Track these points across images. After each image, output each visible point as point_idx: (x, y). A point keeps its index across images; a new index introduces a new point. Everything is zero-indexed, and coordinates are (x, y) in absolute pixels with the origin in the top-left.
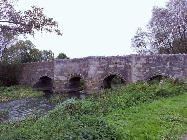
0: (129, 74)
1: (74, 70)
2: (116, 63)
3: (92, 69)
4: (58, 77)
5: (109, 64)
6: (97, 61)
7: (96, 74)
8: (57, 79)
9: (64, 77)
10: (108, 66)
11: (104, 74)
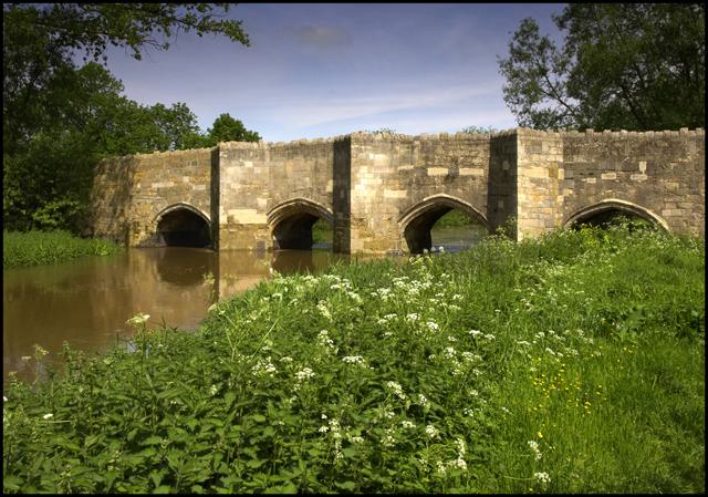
1: (295, 186)
3: (363, 181)
4: (231, 212)
5: (428, 166)
6: (384, 151)
7: (379, 201)
8: (230, 219)
9: (254, 212)
10: (424, 169)
11: (409, 202)
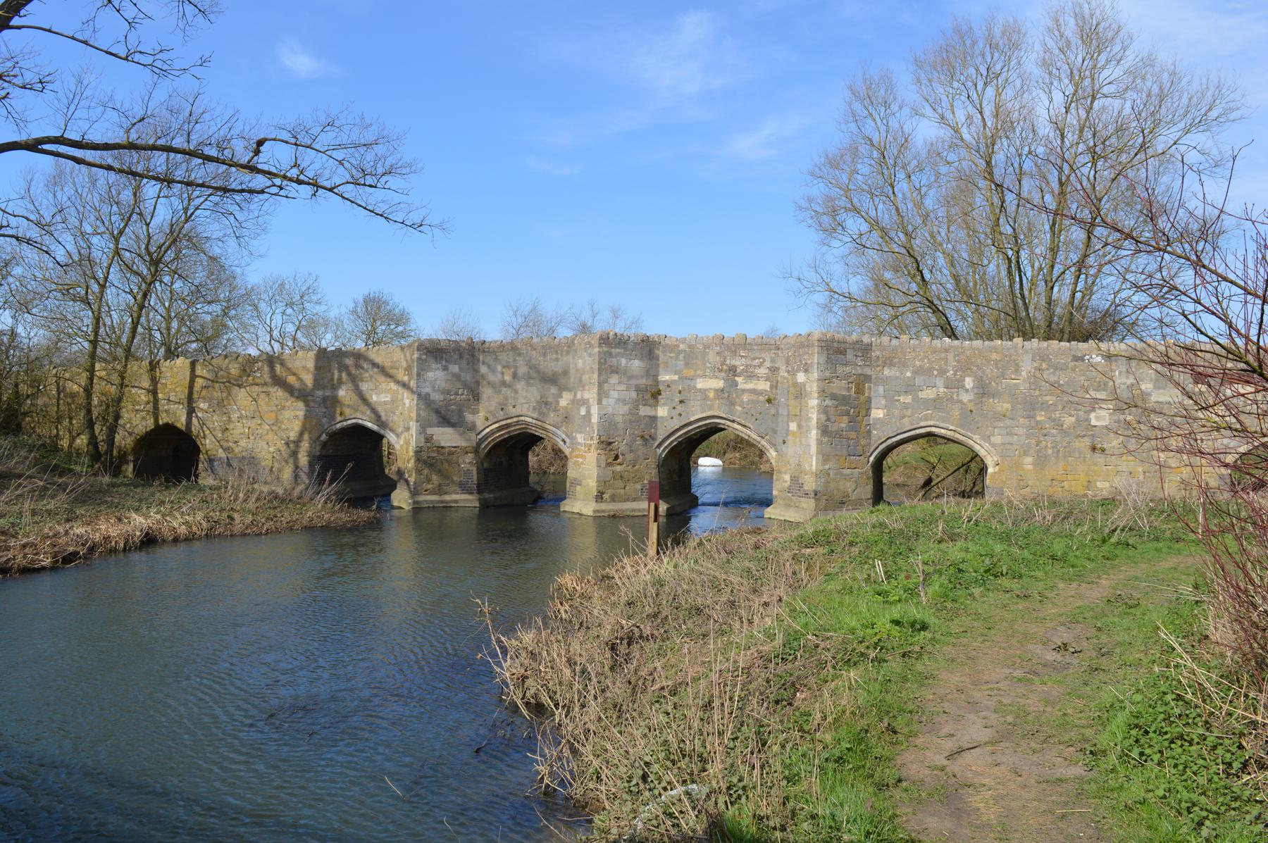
0: (793, 426)
2: (733, 370)
3: (614, 394)
4: (430, 431)
